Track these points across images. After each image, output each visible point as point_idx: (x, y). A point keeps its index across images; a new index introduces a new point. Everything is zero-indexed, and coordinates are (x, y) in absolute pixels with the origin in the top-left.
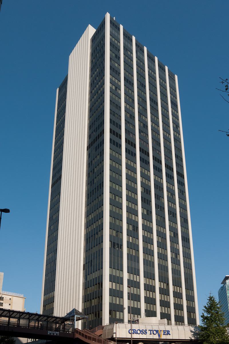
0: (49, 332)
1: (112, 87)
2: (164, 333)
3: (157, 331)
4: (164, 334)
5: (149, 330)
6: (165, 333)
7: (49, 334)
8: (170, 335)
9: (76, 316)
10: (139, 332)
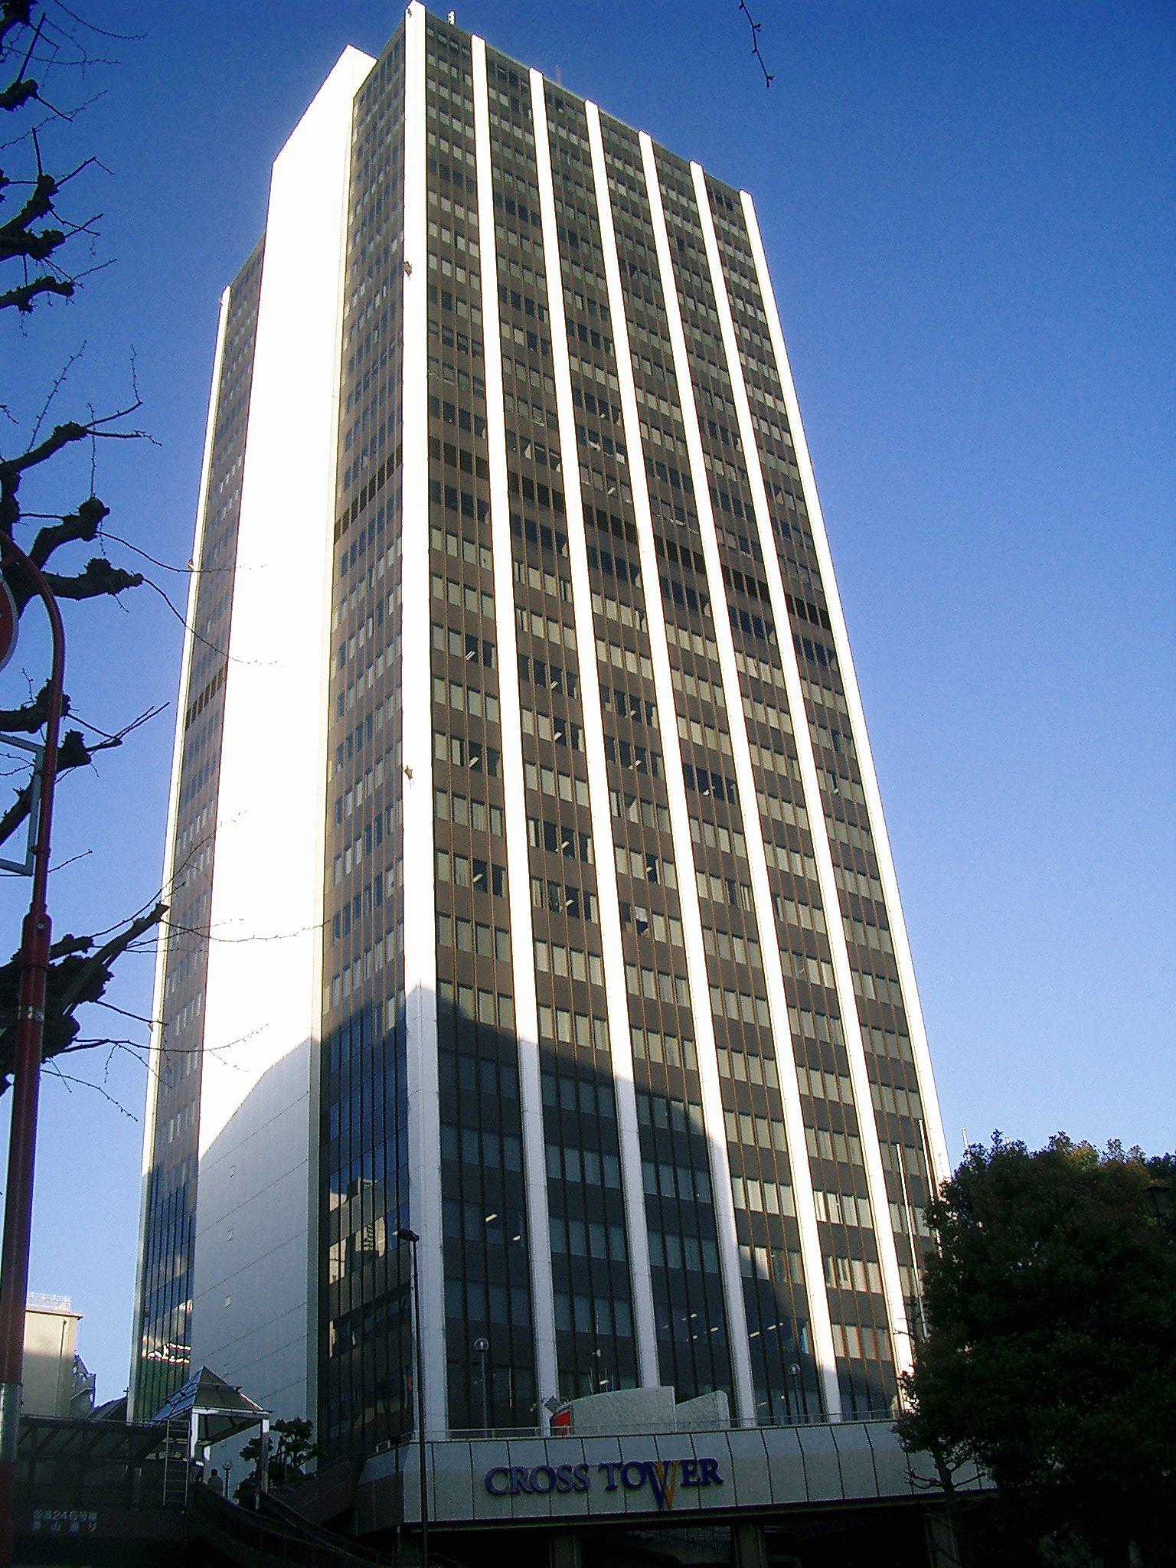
0: (38, 1514)
1: (646, 400)
2: (687, 1474)
3: (646, 1469)
4: (686, 1484)
5: (603, 1467)
6: (693, 1473)
7: (37, 1525)
8: (719, 1482)
9: (197, 1412)
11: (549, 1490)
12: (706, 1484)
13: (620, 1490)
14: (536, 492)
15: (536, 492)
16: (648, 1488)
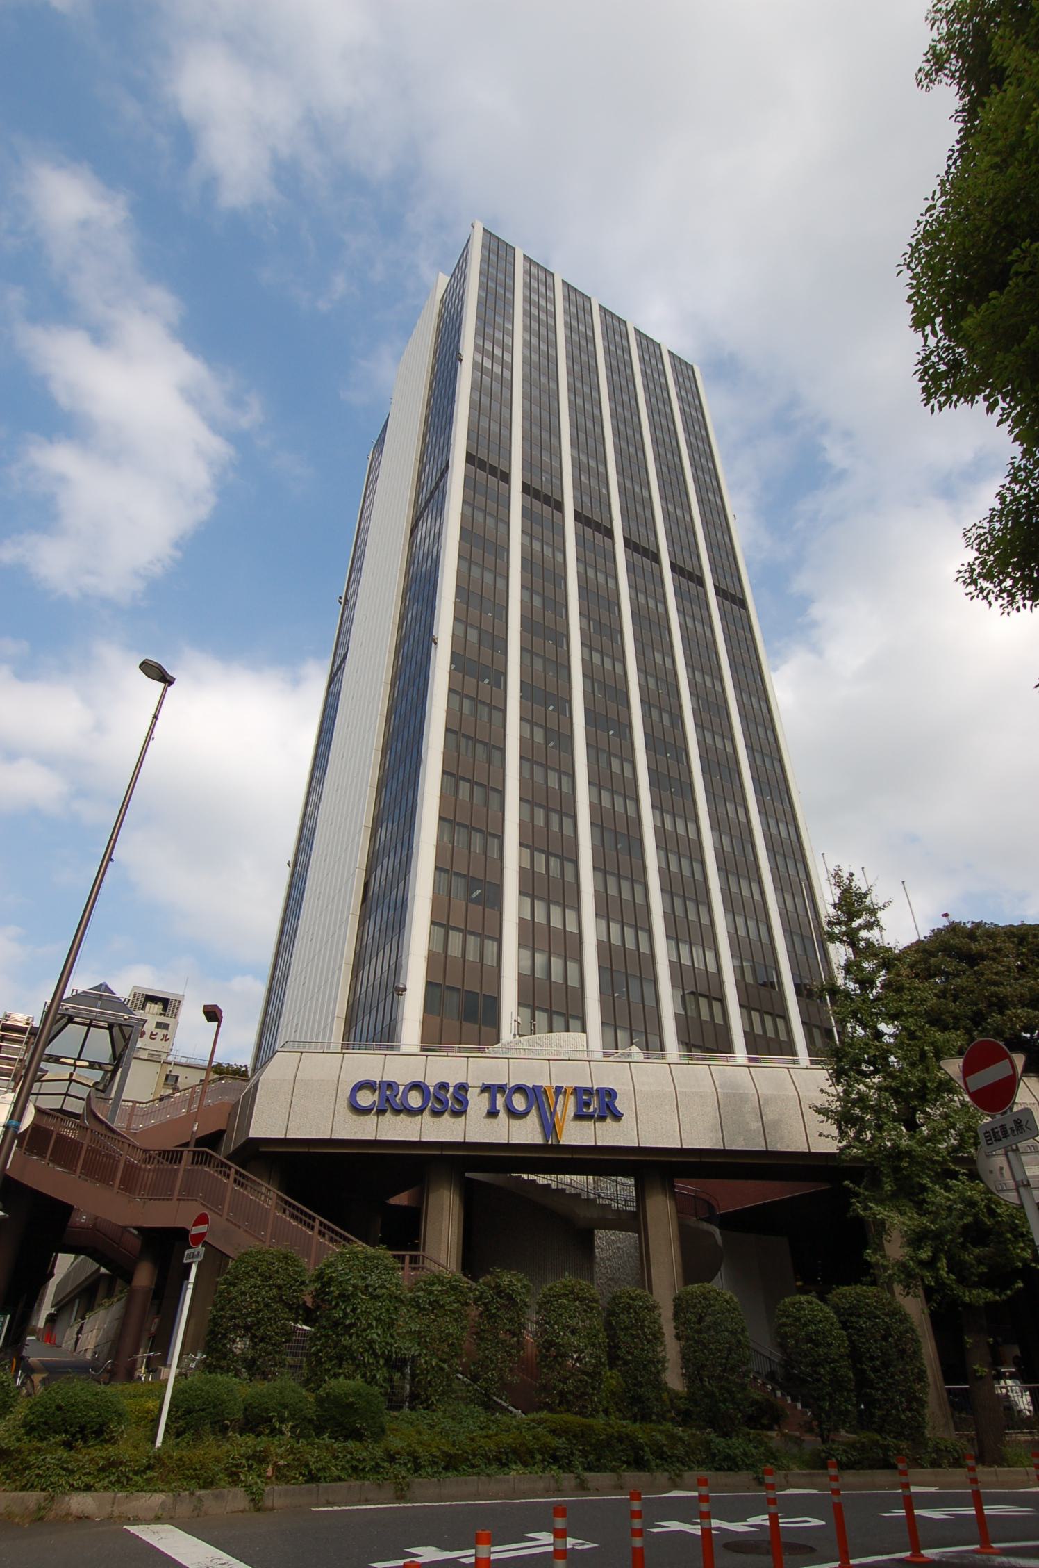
3: (534, 1094)
4: (579, 1117)
5: (486, 1088)
6: (587, 1104)
8: (617, 1117)
10: (415, 1100)
11: (420, 1111)
12: (602, 1118)
13: (503, 1115)
14: (666, 745)
15: (666, 745)
16: (533, 1116)
